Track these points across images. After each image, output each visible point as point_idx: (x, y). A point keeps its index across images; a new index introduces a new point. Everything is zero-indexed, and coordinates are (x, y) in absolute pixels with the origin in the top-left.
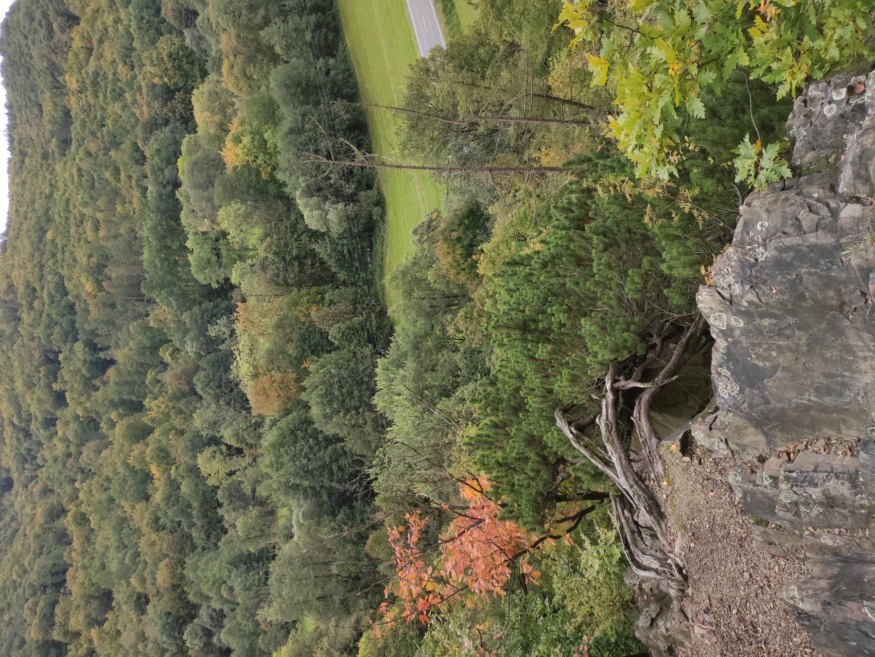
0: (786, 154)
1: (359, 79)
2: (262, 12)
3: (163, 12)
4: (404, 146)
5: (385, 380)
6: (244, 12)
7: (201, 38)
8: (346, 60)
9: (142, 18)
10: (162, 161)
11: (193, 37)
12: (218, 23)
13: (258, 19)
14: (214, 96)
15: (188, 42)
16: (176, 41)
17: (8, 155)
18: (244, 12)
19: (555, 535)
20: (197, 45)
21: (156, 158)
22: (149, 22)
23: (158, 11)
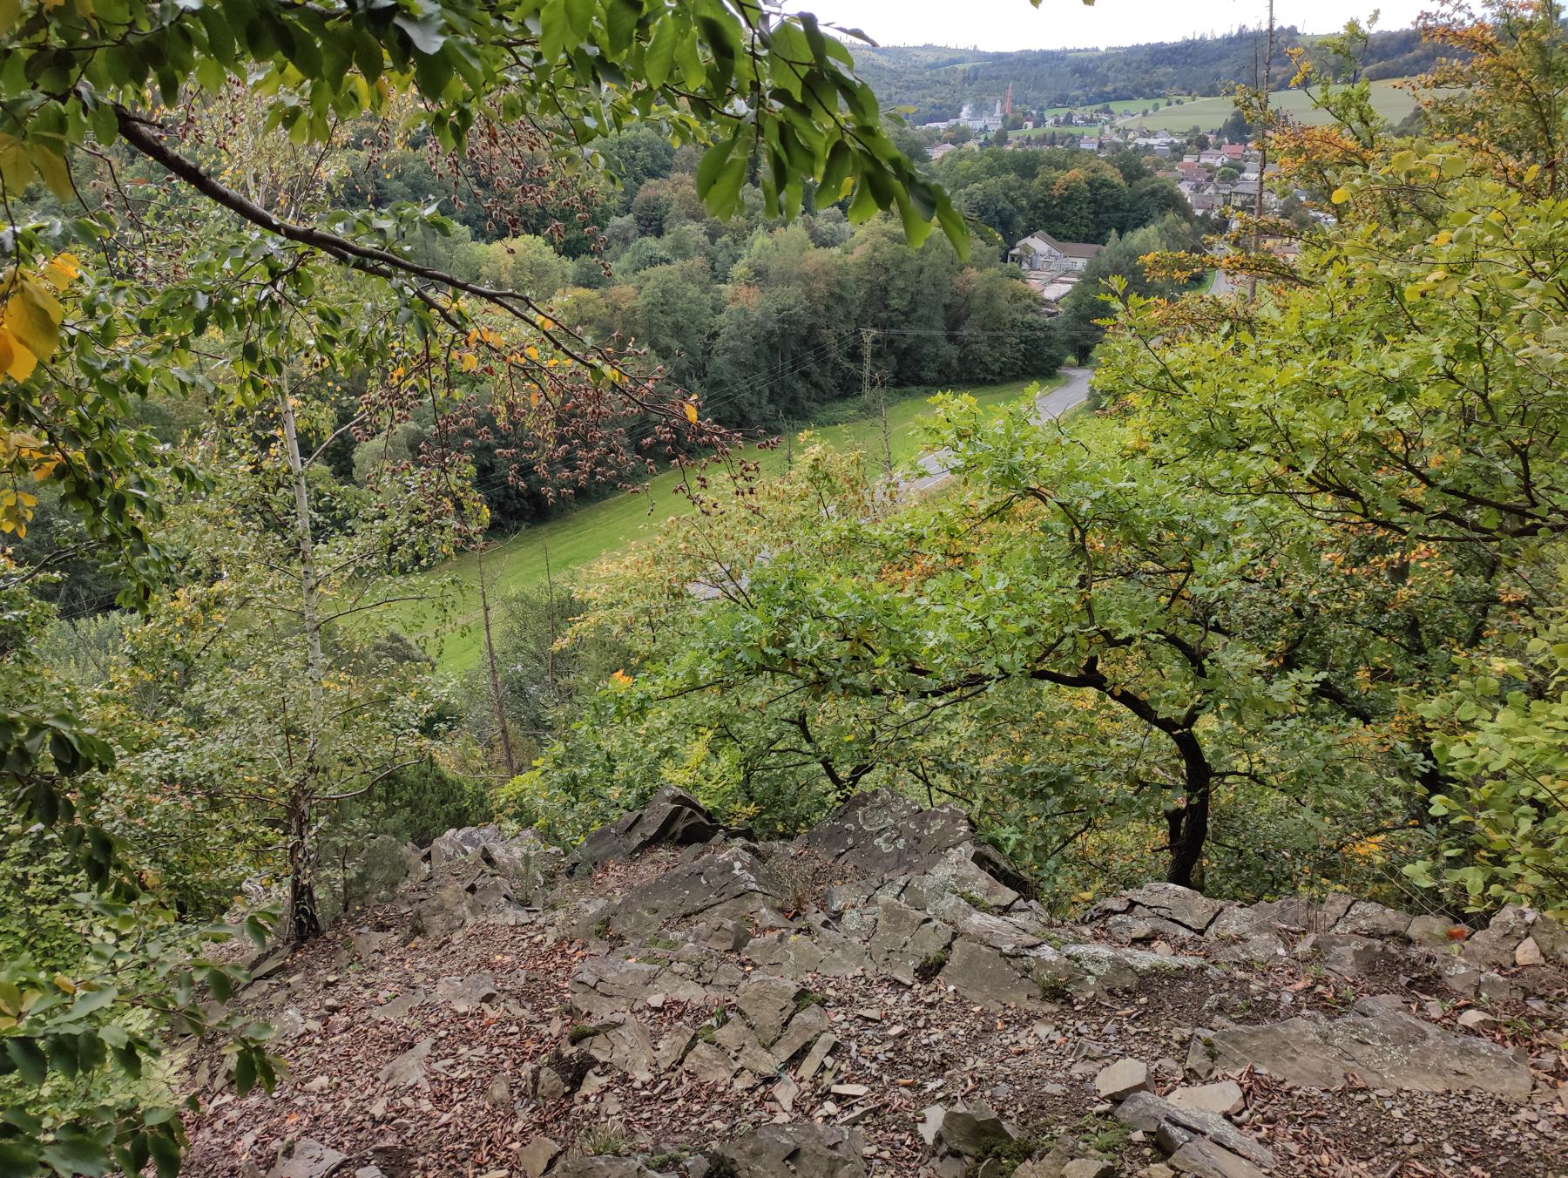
0: (691, 579)
1: (611, 500)
2: (676, 345)
3: (652, 182)
4: (524, 600)
5: (100, 633)
6: (670, 319)
7: (626, 241)
8: (636, 476)
9: (636, 148)
10: (415, 177)
11: (625, 230)
12: (648, 279)
13: (665, 340)
14: (539, 272)
15: (616, 221)
16: (614, 202)
17: (1103, 49)
18: (670, 319)
19: (706, 55)
20: (614, 236)
21: (418, 167)
22: (634, 158)
23: (652, 174)
